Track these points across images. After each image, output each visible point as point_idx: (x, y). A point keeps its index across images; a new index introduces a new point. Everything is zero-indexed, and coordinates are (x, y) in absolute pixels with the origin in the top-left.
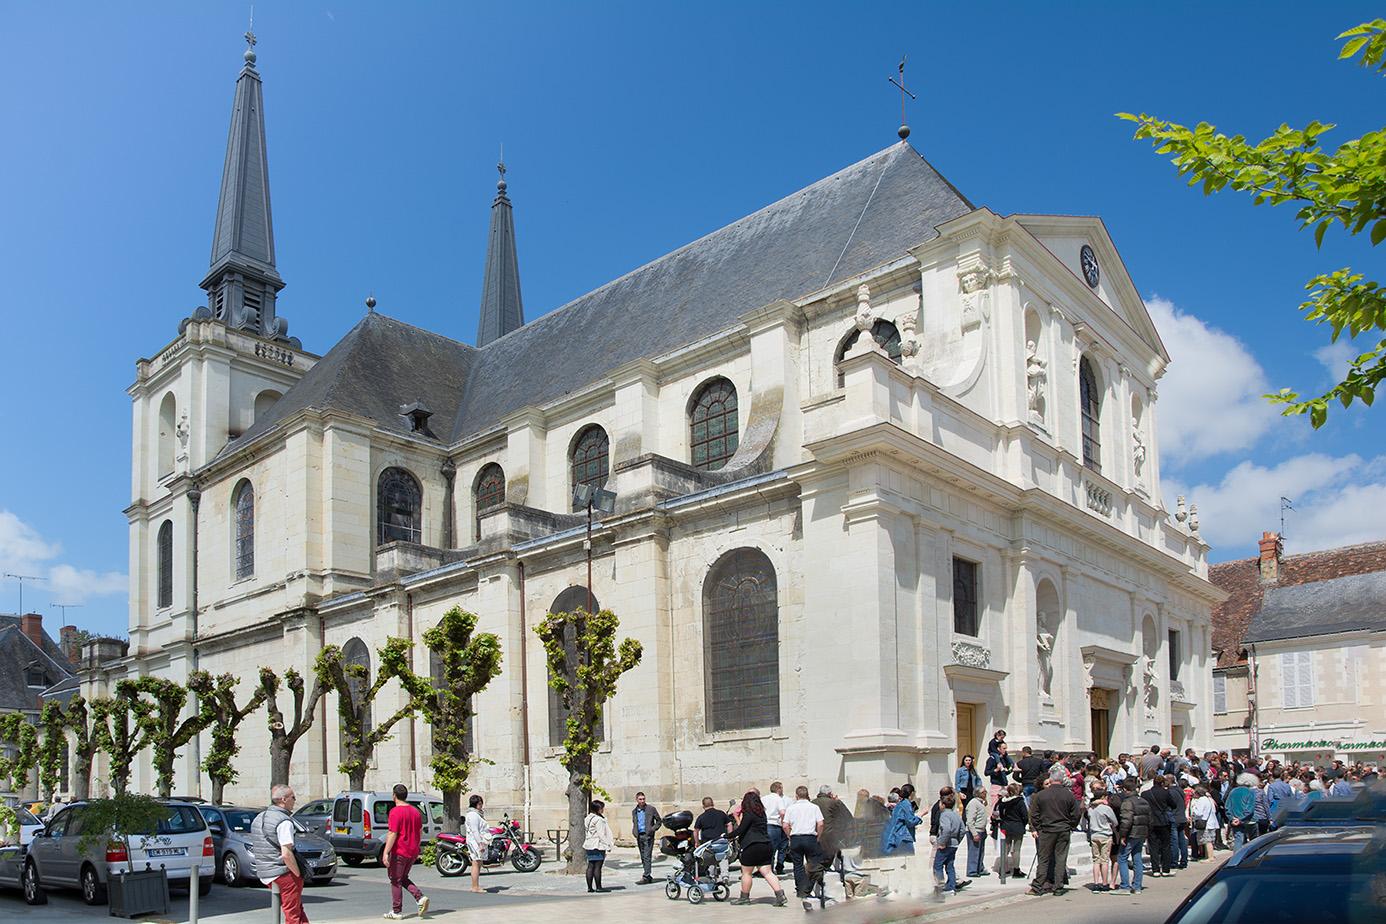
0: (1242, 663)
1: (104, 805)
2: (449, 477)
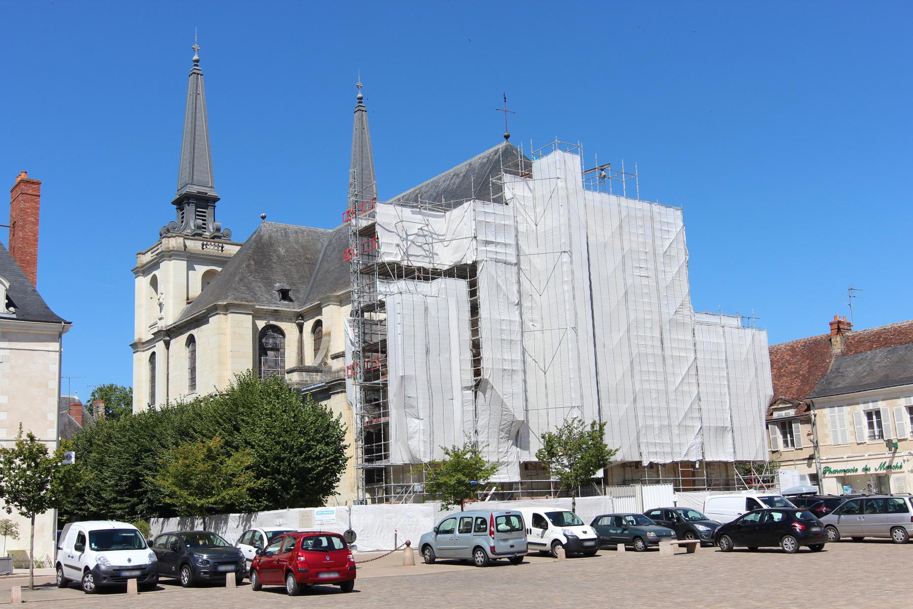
0: (807, 413)
1: (199, 533)
2: (301, 327)
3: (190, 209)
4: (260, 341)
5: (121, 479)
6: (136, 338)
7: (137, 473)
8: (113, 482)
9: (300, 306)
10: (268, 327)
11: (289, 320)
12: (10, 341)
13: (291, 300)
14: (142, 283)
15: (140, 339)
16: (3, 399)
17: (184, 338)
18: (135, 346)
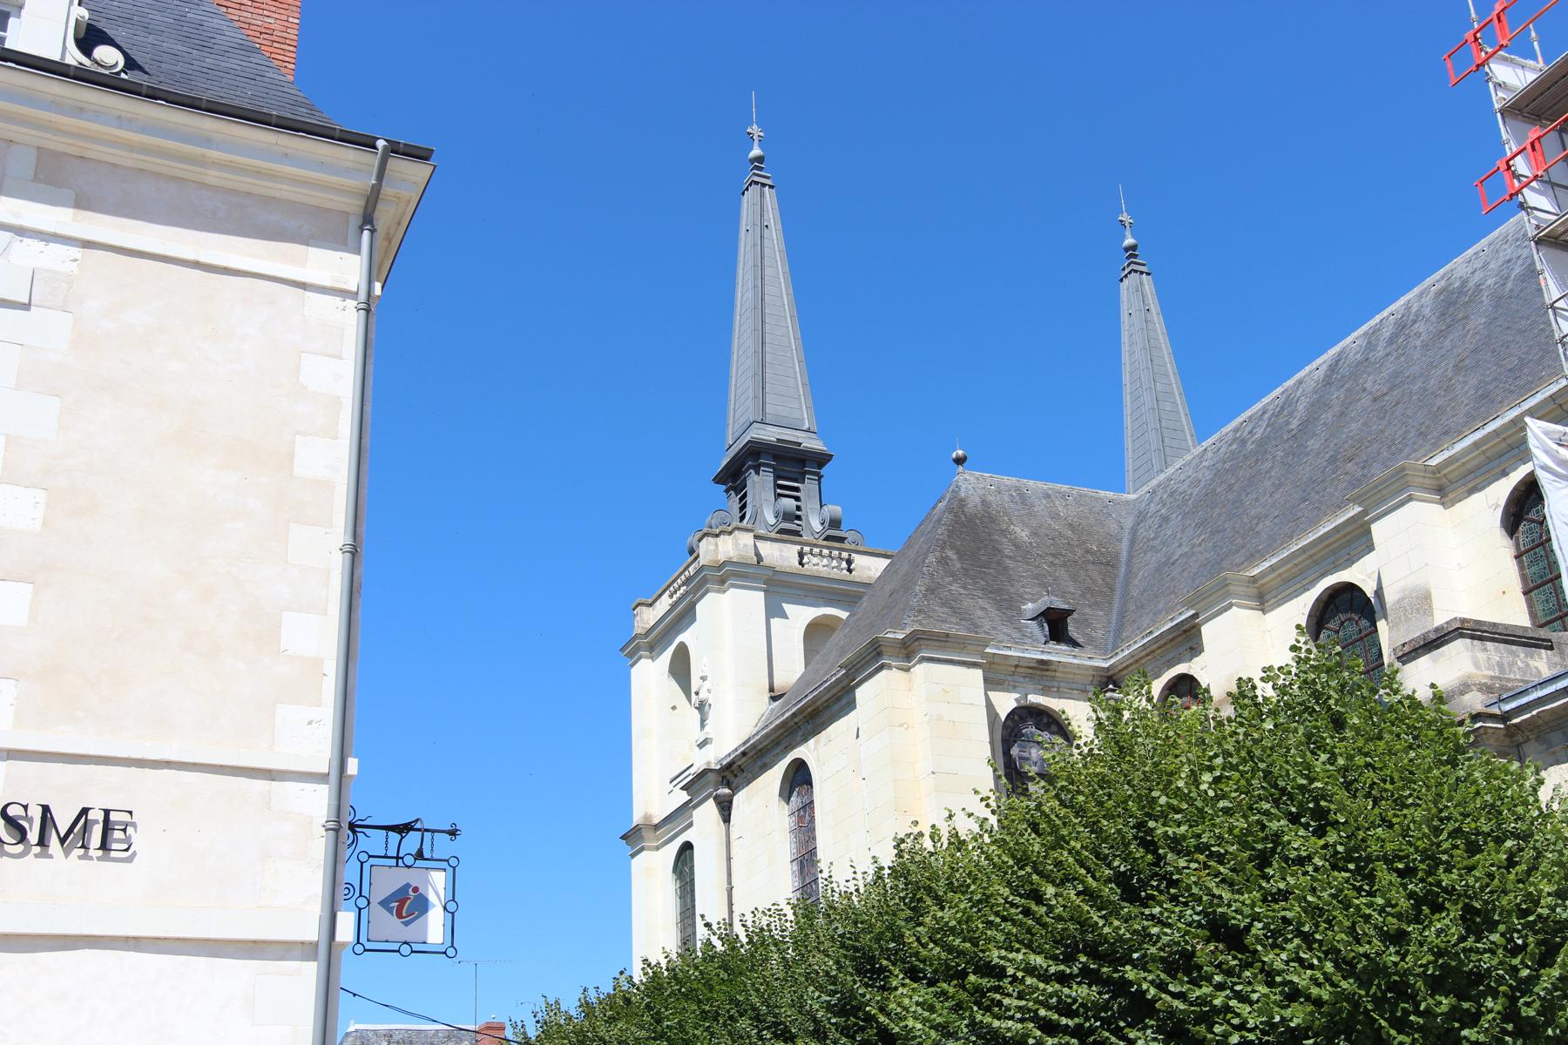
4: (1006, 753)
6: (637, 818)
9: (1106, 651)
11: (1080, 693)
12: (82, 202)
14: (650, 675)
16: (19, 509)
17: (774, 777)
18: (634, 837)
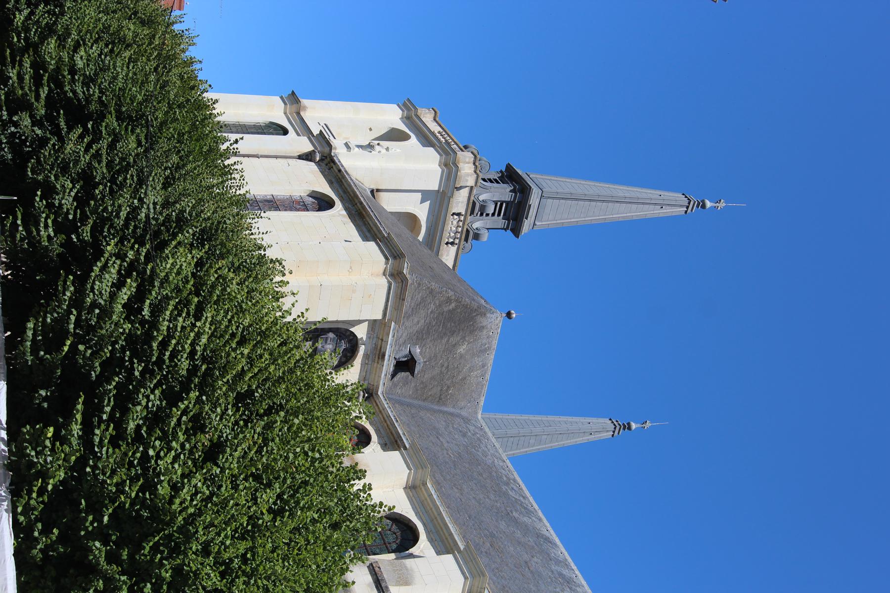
3: (504, 192)
5: (88, 81)
6: (305, 102)
7: (102, 117)
8: (80, 64)
10: (353, 344)
13: (393, 376)
15: (305, 108)
17: (326, 189)
18: (293, 99)
